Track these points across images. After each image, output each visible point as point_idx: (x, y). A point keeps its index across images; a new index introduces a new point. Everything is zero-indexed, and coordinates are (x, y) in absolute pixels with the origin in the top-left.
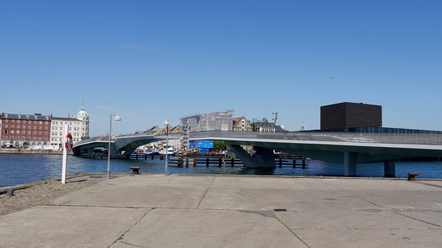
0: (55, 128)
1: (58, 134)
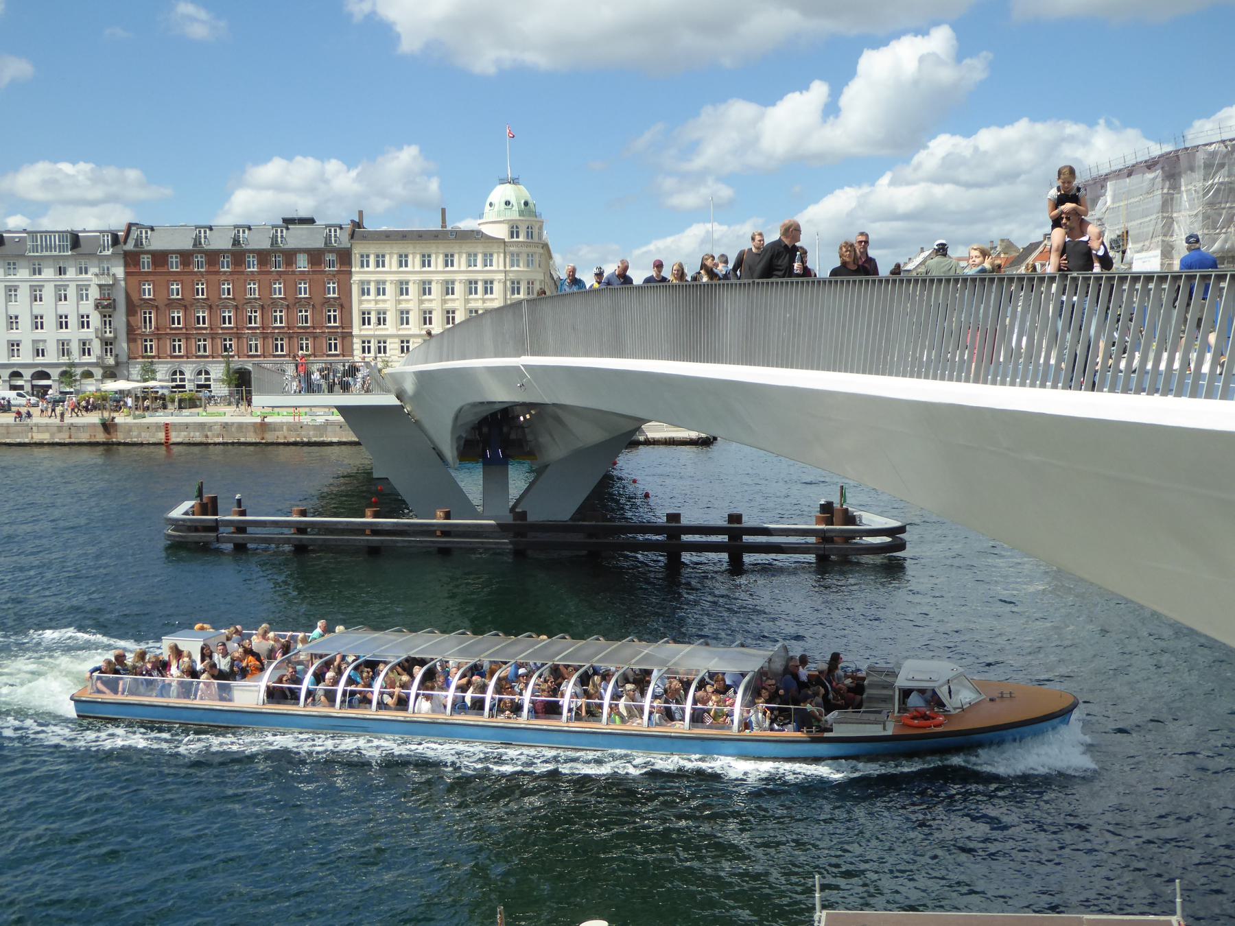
0: (373, 287)
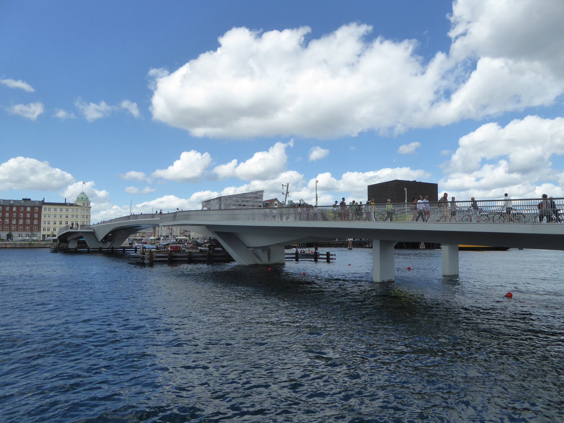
1: (52, 223)
